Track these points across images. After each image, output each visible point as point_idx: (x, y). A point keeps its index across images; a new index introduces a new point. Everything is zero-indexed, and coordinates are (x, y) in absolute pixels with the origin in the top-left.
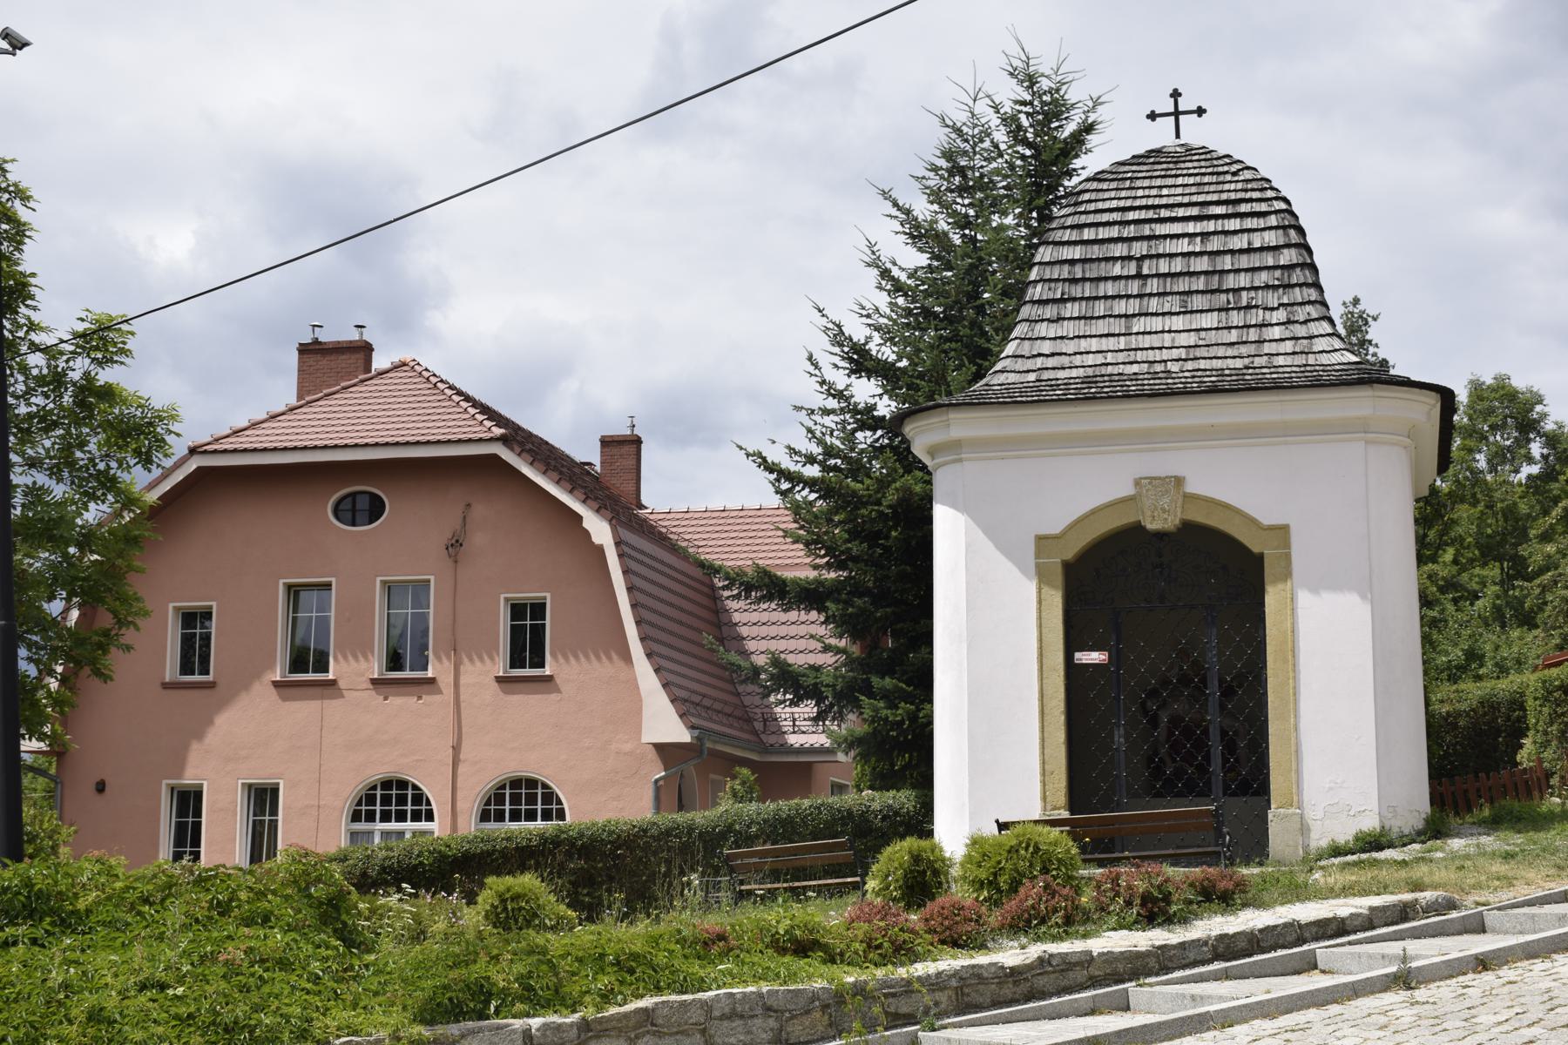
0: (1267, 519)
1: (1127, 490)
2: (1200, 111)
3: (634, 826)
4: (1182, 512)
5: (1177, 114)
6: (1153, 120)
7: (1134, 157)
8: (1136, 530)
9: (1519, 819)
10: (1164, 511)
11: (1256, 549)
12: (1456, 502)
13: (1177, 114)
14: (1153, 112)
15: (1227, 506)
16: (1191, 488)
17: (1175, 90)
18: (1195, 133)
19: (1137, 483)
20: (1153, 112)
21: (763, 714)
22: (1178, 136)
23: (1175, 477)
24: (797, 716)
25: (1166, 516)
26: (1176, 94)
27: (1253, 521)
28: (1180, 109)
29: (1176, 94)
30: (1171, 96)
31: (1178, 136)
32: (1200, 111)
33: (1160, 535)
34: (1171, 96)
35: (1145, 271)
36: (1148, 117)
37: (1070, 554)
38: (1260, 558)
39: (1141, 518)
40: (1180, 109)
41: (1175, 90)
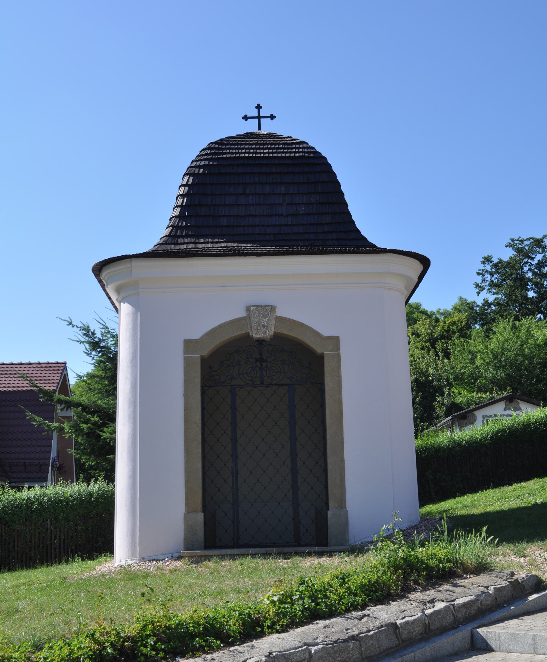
0: (326, 332)
1: (242, 313)
2: (272, 117)
3: (24, 500)
4: (275, 328)
5: (259, 117)
6: (246, 120)
7: (237, 135)
8: (247, 337)
9: (317, 334)
10: (264, 326)
11: (319, 351)
12: (534, 289)
13: (259, 117)
14: (246, 116)
15: (302, 325)
16: (281, 312)
17: (259, 105)
18: (268, 127)
19: (248, 309)
20: (246, 116)
21: (10, 463)
22: (260, 129)
23: (271, 306)
24: (27, 464)
25: (265, 329)
26: (259, 107)
27: (317, 334)
28: (261, 115)
29: (259, 107)
30: (256, 107)
31: (260, 129)
32: (272, 117)
33: (261, 342)
34: (256, 107)
35: (248, 191)
36: (243, 118)
37: (206, 352)
38: (321, 358)
39: (249, 331)
40: (261, 115)
41: (259, 105)
